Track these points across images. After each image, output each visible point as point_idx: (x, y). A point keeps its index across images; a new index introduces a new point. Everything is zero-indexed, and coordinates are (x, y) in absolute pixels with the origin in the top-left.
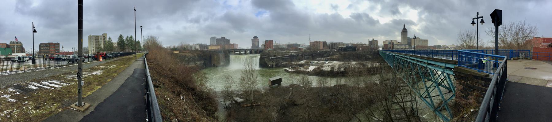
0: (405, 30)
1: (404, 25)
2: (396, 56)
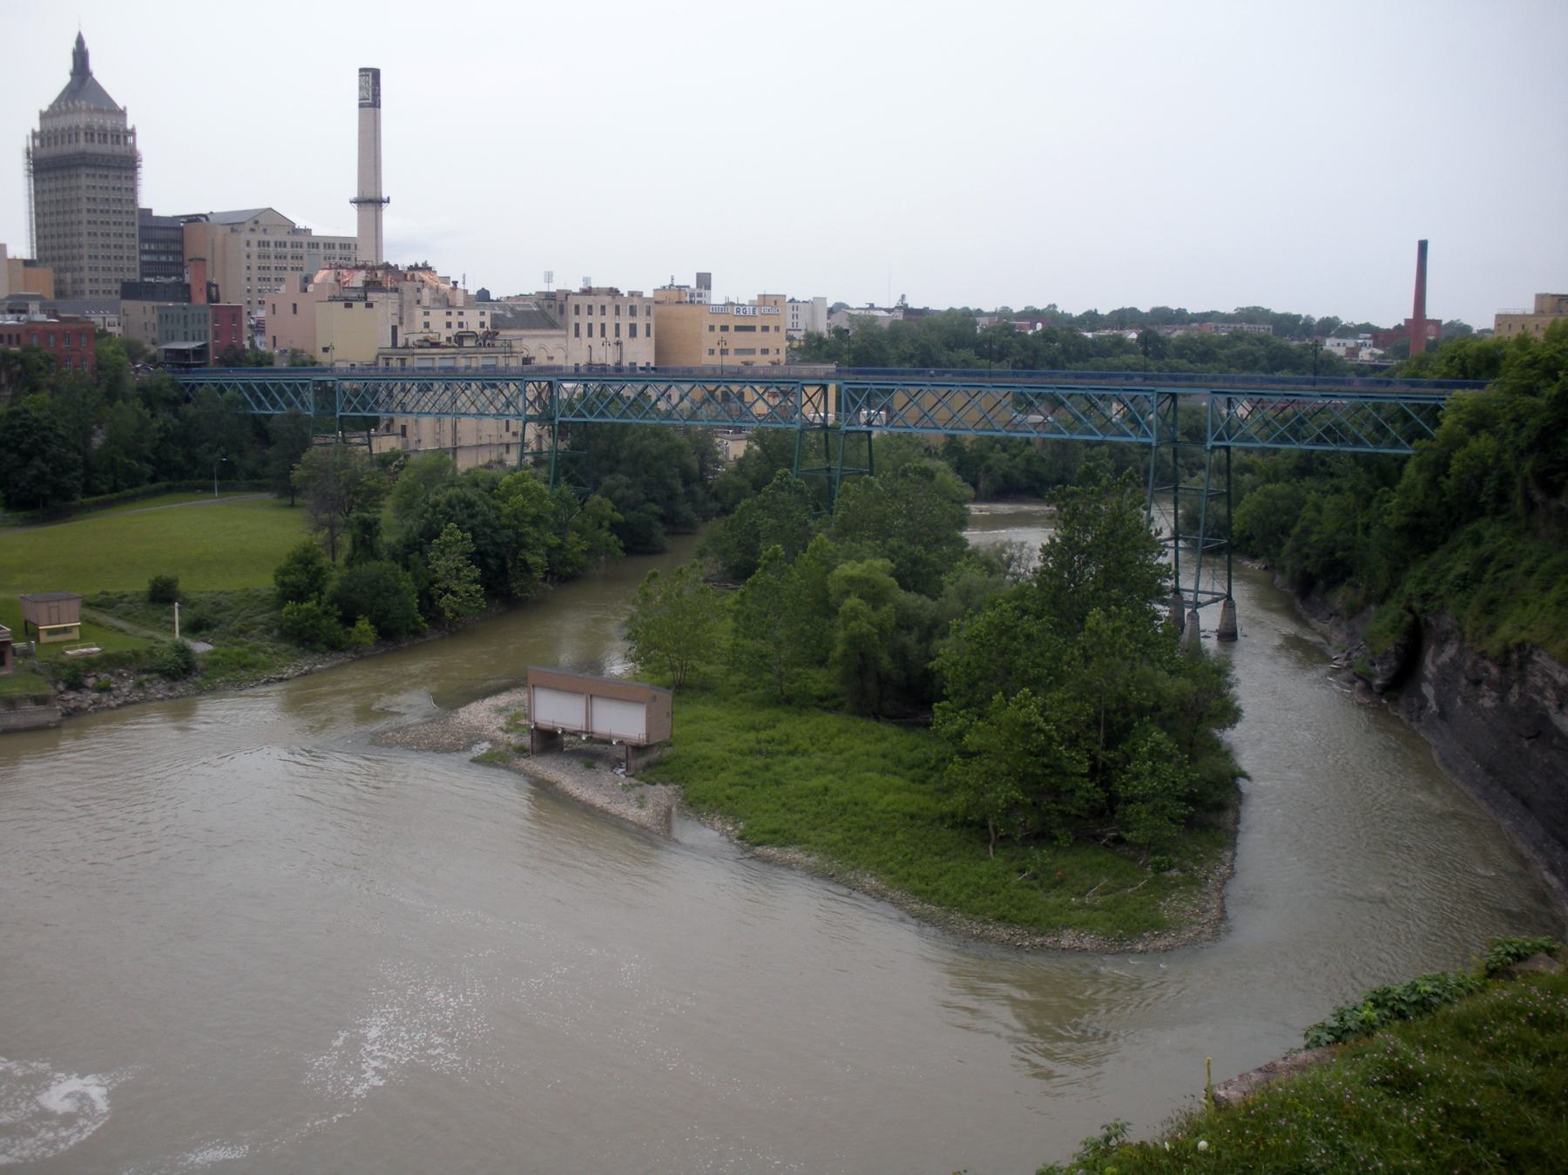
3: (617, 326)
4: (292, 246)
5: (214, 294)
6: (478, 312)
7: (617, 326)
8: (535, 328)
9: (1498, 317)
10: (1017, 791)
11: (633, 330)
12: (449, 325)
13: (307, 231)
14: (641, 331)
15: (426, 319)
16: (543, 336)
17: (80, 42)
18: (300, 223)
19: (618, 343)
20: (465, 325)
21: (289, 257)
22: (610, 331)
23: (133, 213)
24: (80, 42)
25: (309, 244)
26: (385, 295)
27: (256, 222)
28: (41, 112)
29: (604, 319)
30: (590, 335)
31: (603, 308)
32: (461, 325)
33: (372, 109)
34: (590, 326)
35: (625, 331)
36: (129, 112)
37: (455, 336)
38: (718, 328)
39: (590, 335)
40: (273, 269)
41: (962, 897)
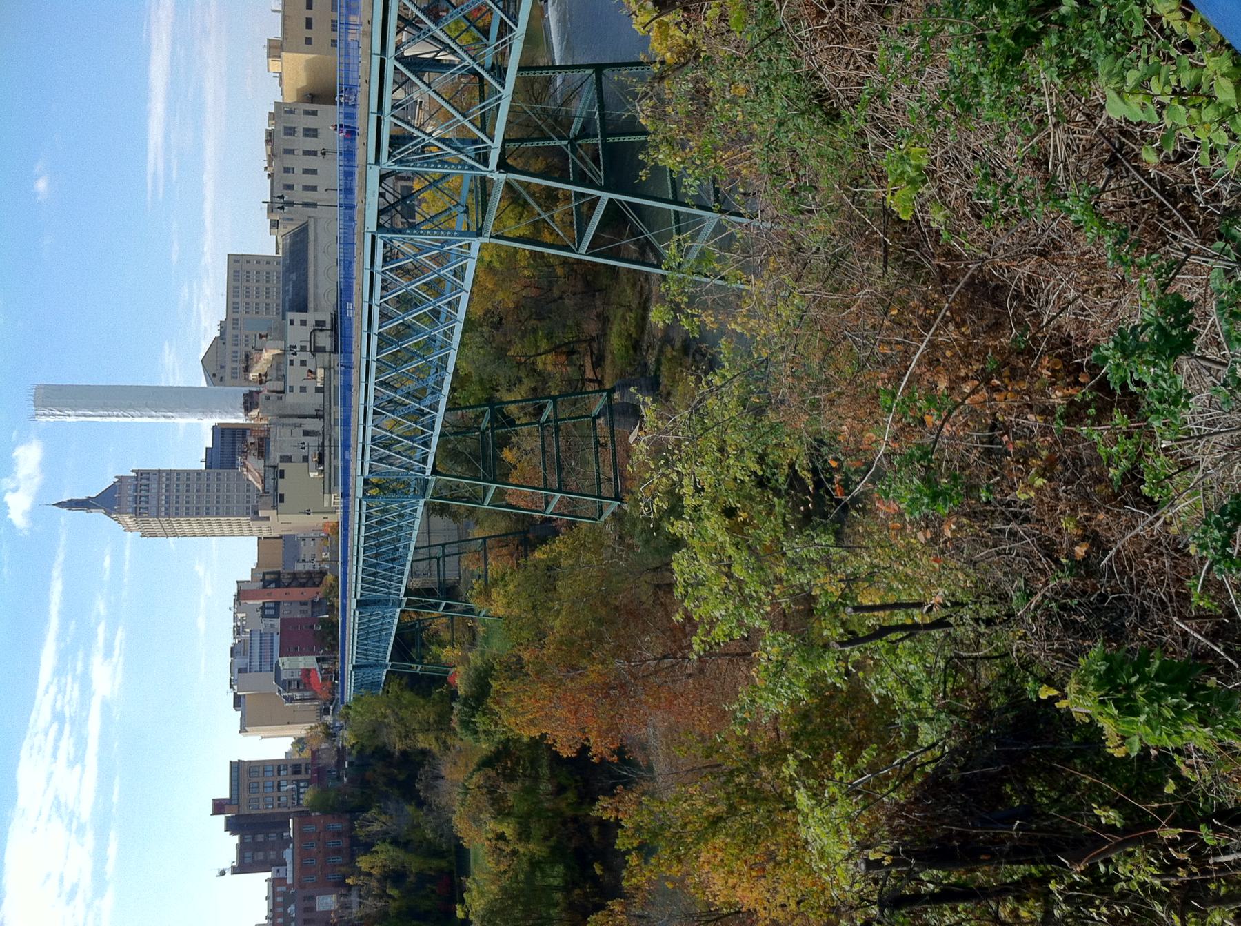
2: (358, 597)
3: (306, 153)
4: (237, 345)
7: (306, 153)
8: (306, 260)
11: (311, 133)
13: (222, 325)
14: (311, 122)
15: (296, 389)
16: (315, 249)
17: (61, 505)
19: (324, 154)
20: (303, 344)
22: (312, 162)
23: (208, 474)
24: (61, 505)
25: (234, 328)
27: (214, 375)
29: (299, 171)
30: (314, 189)
31: (287, 170)
32: (303, 349)
34: (306, 188)
35: (311, 144)
36: (120, 475)
38: (309, 33)
39: (314, 189)
40: (257, 300)
41: (1084, 168)
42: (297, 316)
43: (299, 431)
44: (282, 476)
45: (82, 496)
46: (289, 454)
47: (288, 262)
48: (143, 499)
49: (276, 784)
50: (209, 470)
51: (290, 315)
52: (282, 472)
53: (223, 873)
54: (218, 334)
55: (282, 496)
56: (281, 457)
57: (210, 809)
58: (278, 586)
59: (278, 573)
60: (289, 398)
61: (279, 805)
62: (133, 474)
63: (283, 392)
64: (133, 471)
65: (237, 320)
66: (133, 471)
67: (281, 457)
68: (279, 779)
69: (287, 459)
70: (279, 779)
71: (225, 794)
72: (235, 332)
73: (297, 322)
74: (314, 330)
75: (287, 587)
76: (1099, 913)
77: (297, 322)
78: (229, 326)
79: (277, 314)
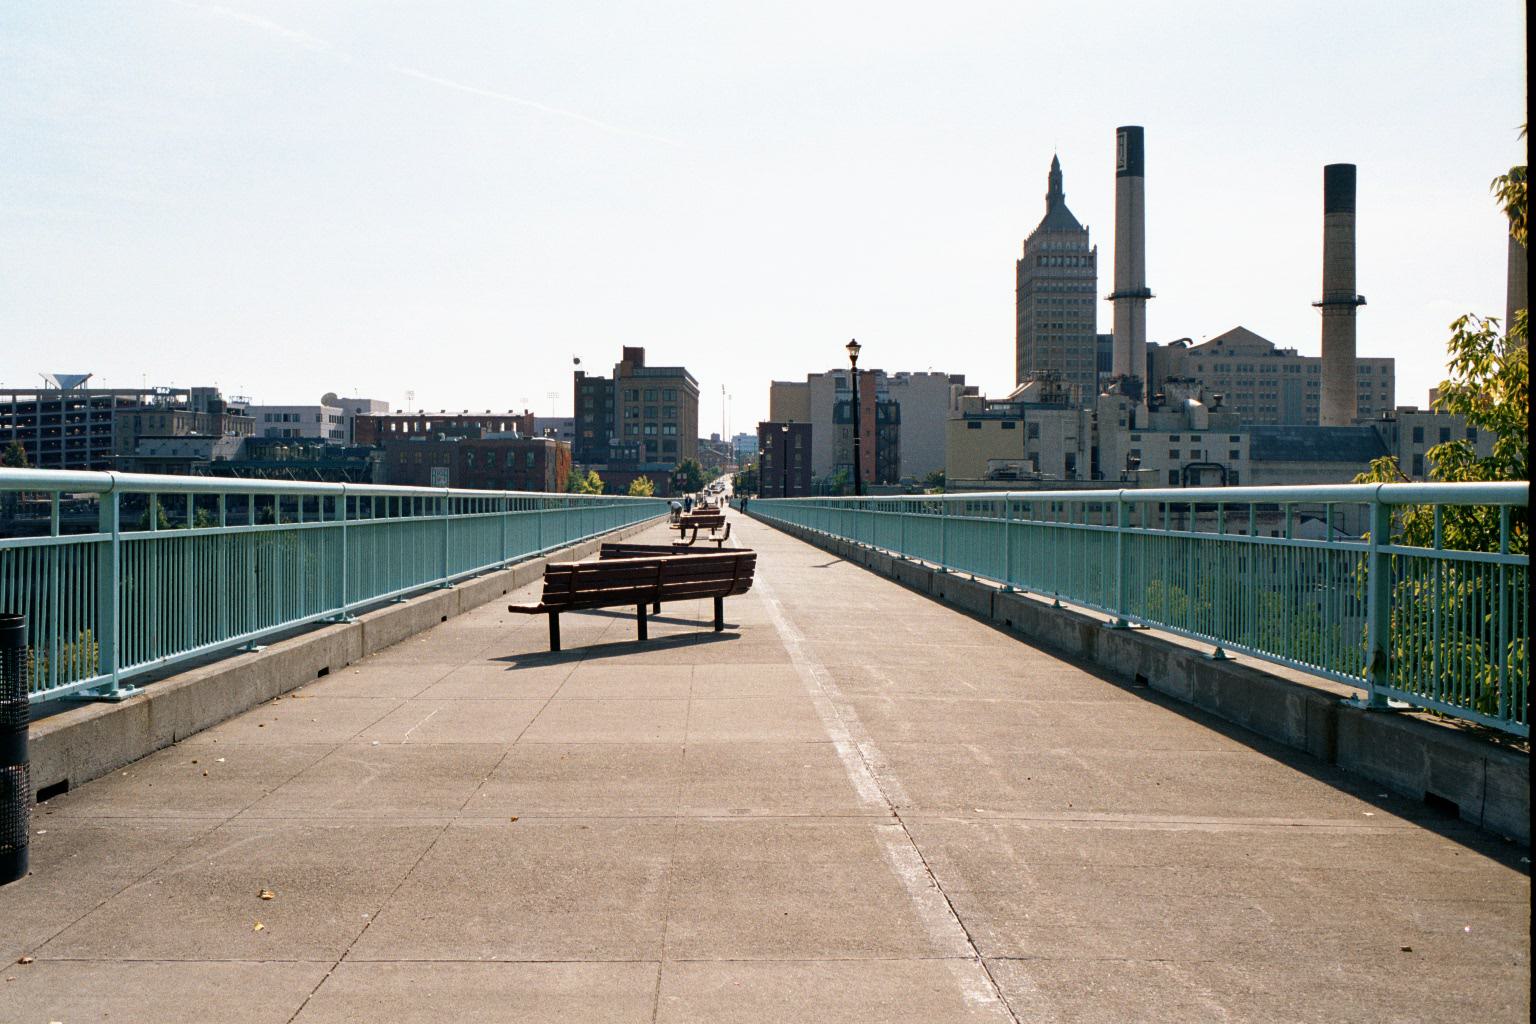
0: (1070, 243)
1: (1055, 177)
5: (893, 415)
6: (1227, 436)
9: (678, 375)
10: (976, 1004)
12: (1174, 454)
17: (1055, 163)
18: (1280, 345)
20: (1203, 454)
21: (1257, 383)
23: (1091, 338)
24: (1055, 163)
26: (1055, 412)
28: (1018, 261)
33: (1128, 178)
37: (1185, 469)
42: (1244, 445)
43: (1072, 447)
44: (1005, 426)
45: (1066, 188)
46: (1041, 435)
47: (149, 399)
48: (1074, 260)
49: (653, 421)
50: (1095, 339)
51: (1245, 438)
52: (1012, 426)
53: (577, 361)
54: (1278, 346)
55: (978, 426)
56: (1037, 425)
57: (630, 345)
58: (878, 421)
59: (898, 421)
60: (1123, 437)
61: (629, 425)
62: (1091, 248)
63: (1132, 426)
64: (1095, 247)
65: (1298, 371)
66: (1095, 247)
67: (1037, 425)
68: (660, 425)
69: (1034, 432)
70: (660, 425)
71: (651, 361)
72: (1280, 368)
73: (1235, 446)
74: (1223, 468)
75: (878, 434)
76: (1368, 1023)
77: (1235, 446)
78: (1288, 361)
79: (1308, 423)
